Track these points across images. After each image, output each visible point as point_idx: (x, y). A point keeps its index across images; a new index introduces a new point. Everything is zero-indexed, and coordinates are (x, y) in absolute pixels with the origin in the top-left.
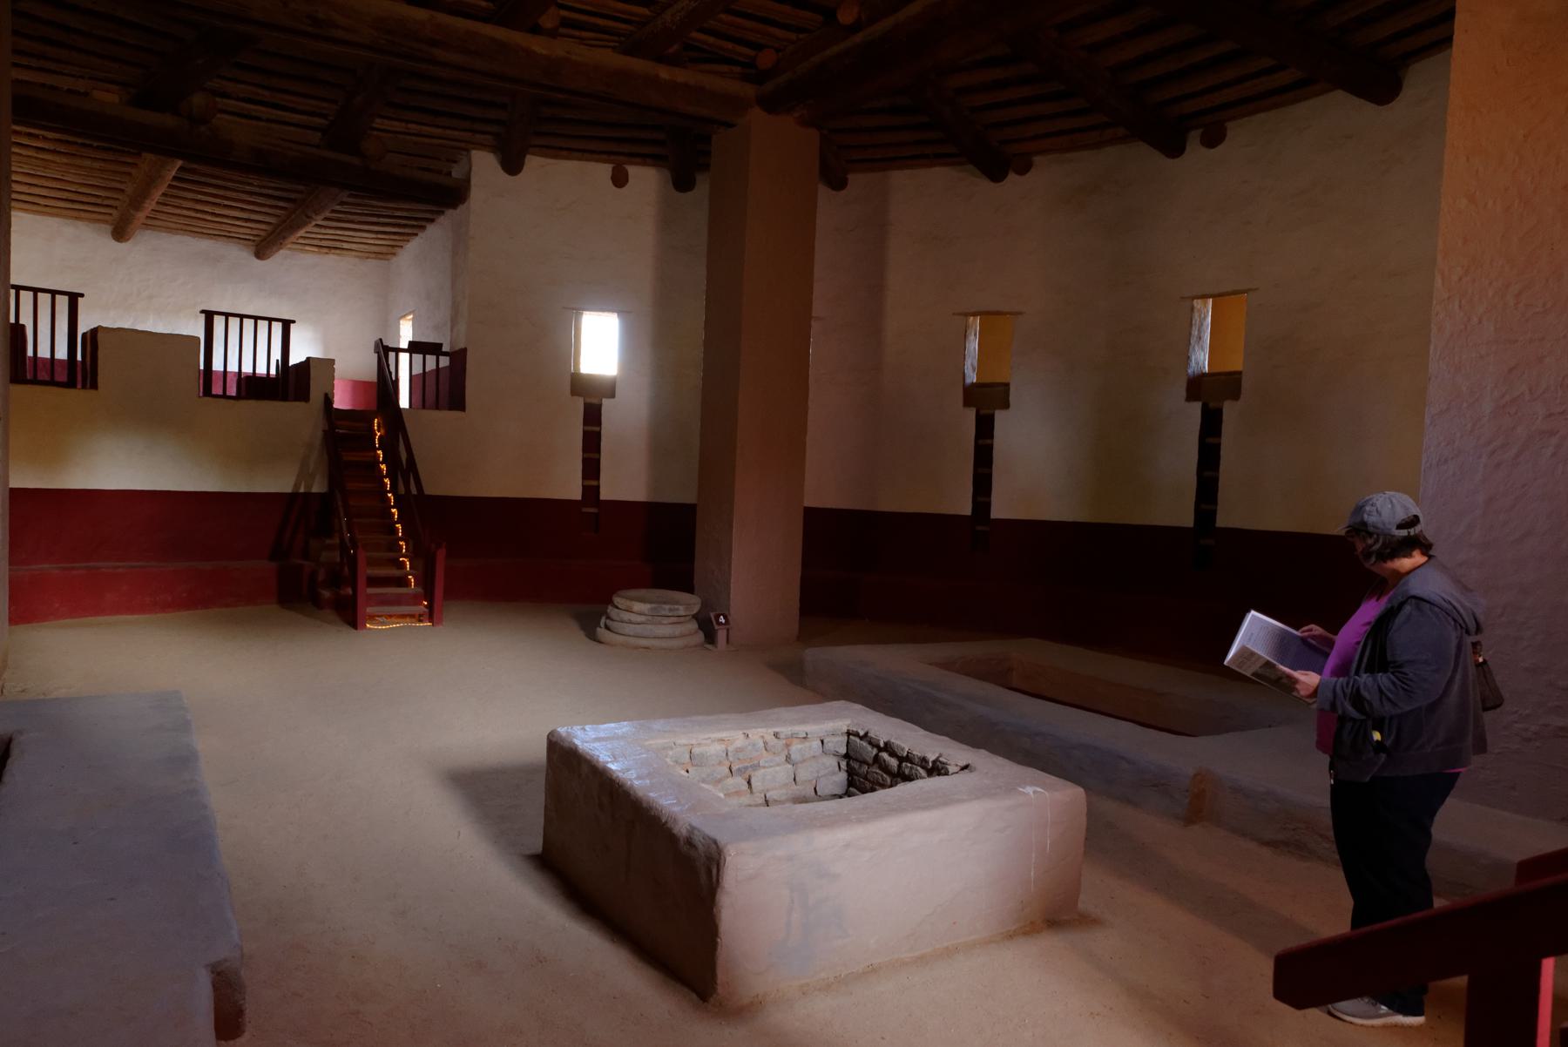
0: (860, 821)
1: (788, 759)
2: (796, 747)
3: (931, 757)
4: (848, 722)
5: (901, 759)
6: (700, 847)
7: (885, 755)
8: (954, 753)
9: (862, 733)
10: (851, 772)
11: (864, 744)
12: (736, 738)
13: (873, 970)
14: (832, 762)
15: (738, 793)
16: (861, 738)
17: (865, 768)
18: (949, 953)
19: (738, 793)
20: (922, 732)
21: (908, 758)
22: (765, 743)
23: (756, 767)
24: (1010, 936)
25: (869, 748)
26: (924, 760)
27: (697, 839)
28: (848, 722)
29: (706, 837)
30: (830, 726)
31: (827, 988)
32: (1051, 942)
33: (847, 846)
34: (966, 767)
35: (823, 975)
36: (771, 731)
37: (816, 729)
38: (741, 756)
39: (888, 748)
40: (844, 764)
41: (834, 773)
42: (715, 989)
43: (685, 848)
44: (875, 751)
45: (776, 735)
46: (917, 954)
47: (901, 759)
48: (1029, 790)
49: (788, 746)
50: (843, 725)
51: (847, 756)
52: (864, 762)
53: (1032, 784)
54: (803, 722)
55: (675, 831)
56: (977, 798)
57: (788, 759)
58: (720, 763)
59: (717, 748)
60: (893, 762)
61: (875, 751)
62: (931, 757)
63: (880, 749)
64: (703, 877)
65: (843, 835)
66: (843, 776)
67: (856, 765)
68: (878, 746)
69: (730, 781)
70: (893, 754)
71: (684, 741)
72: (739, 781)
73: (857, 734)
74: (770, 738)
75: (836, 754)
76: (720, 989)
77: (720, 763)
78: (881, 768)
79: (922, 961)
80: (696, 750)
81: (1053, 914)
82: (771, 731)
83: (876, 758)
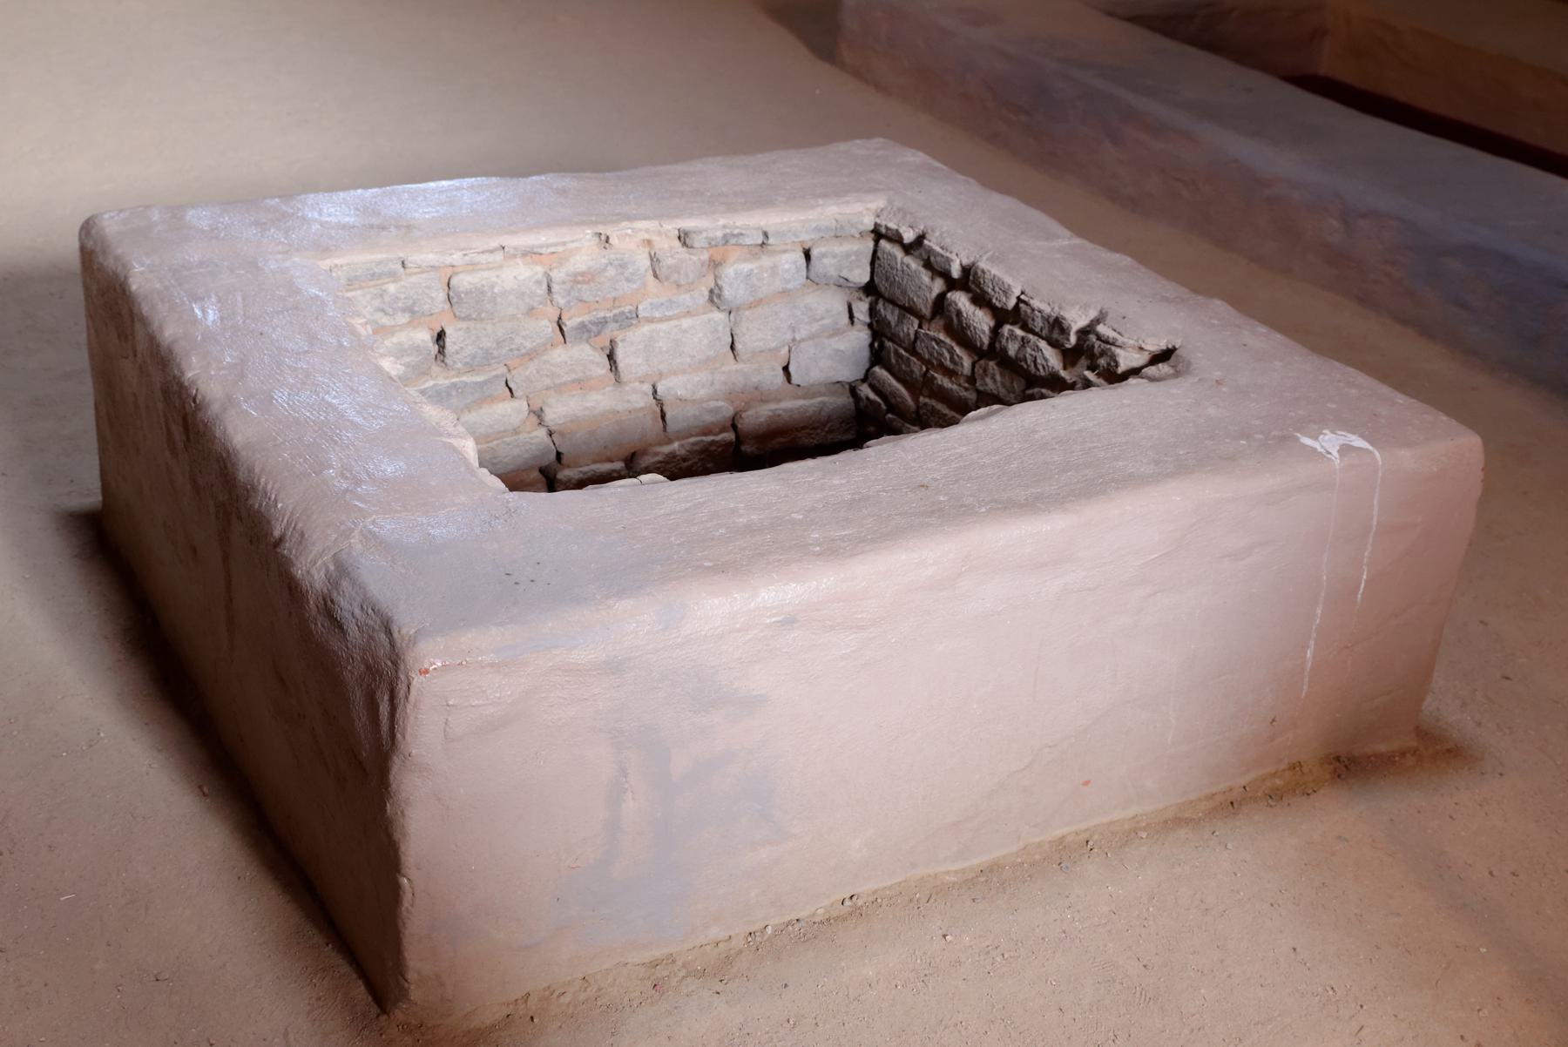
0: (832, 551)
1: (715, 297)
2: (735, 270)
3: (1077, 320)
4: (879, 202)
5: (1002, 316)
6: (352, 629)
7: (961, 300)
8: (1138, 315)
9: (909, 236)
10: (878, 330)
11: (914, 264)
12: (580, 249)
13: (855, 911)
14: (832, 305)
15: (582, 384)
16: (908, 249)
17: (911, 326)
18: (1065, 855)
19: (582, 384)
20: (1066, 239)
21: (1016, 315)
22: (654, 259)
23: (631, 319)
24: (1230, 805)
25: (925, 276)
26: (1057, 325)
27: (347, 606)
28: (879, 202)
29: (370, 606)
30: (830, 212)
31: (719, 969)
32: (1341, 817)
33: (789, 622)
34: (1164, 356)
35: (715, 932)
36: (672, 227)
37: (790, 222)
38: (586, 292)
39: (969, 281)
40: (862, 309)
41: (836, 332)
42: (403, 994)
43: (320, 626)
44: (938, 286)
45: (683, 238)
46: (977, 861)
47: (1002, 316)
48: (1330, 442)
49: (715, 264)
50: (864, 211)
51: (870, 289)
52: (909, 310)
53: (1342, 423)
54: (761, 202)
55: (299, 572)
56: (1182, 470)
57: (715, 297)
58: (531, 311)
59: (520, 275)
60: (980, 321)
61: (938, 286)
62: (1077, 320)
63: (952, 284)
64: (360, 718)
65: (776, 593)
66: (860, 338)
67: (890, 314)
68: (945, 275)
69: (560, 355)
70: (981, 300)
71: (430, 258)
72: (588, 356)
73: (896, 238)
74: (667, 245)
75: (842, 284)
76: (415, 994)
77: (531, 311)
78: (949, 329)
79: (991, 880)
80: (463, 281)
81: (1356, 741)
82: (672, 227)
83: (940, 304)
